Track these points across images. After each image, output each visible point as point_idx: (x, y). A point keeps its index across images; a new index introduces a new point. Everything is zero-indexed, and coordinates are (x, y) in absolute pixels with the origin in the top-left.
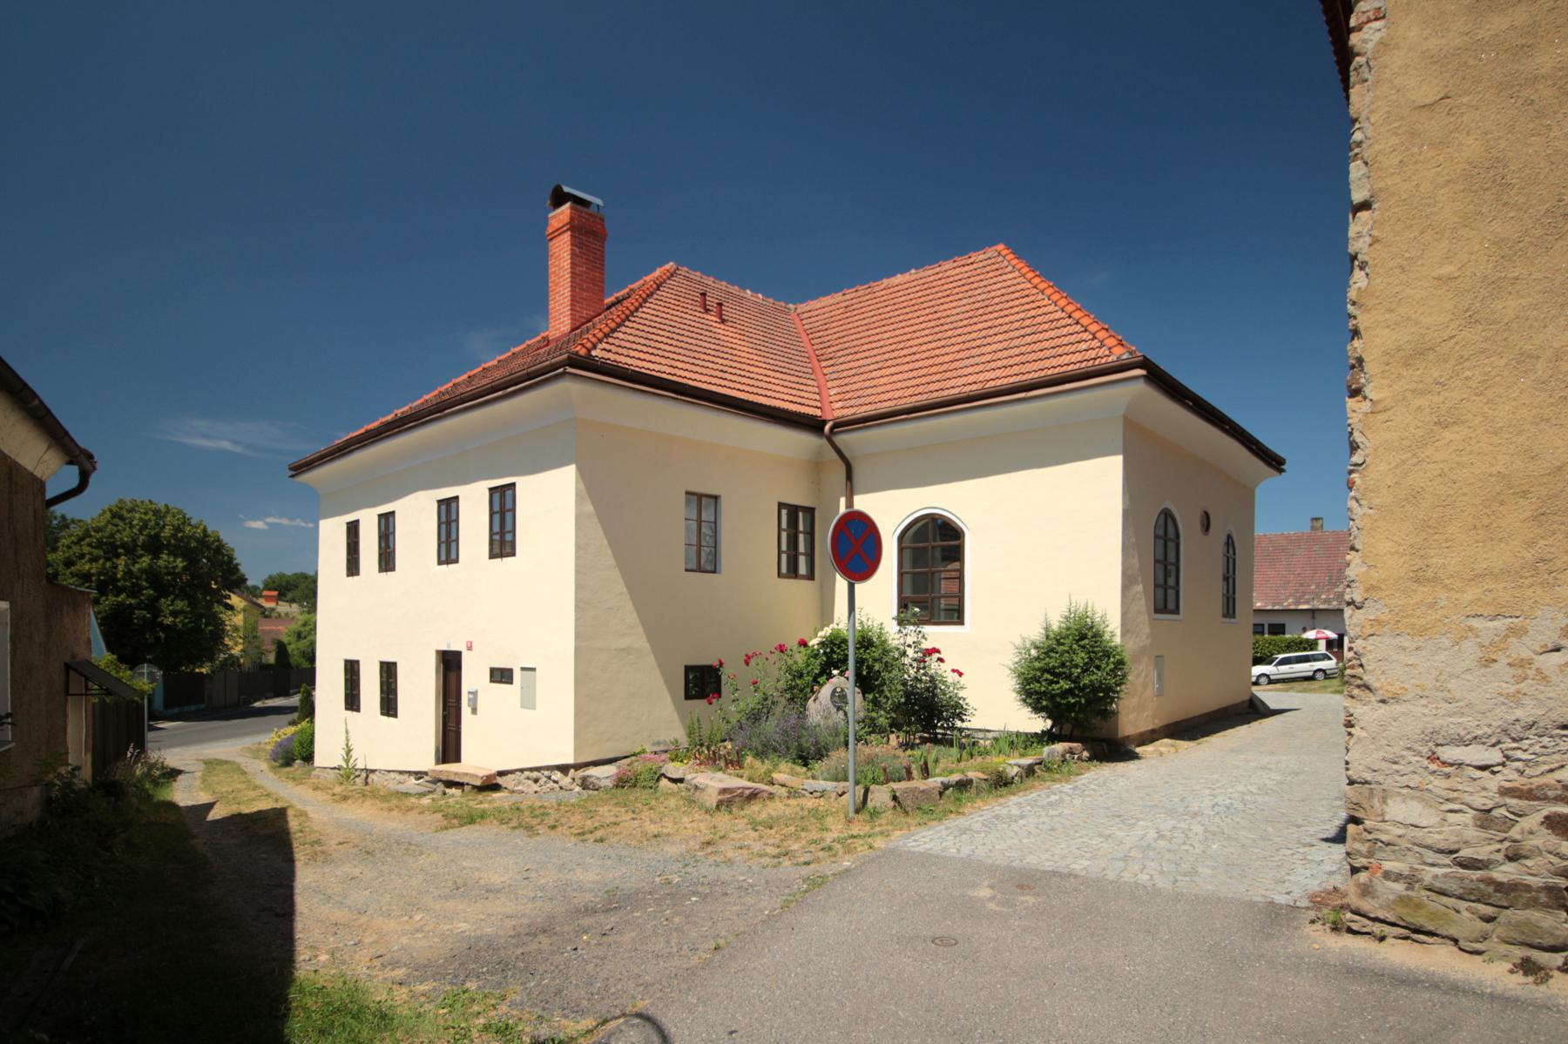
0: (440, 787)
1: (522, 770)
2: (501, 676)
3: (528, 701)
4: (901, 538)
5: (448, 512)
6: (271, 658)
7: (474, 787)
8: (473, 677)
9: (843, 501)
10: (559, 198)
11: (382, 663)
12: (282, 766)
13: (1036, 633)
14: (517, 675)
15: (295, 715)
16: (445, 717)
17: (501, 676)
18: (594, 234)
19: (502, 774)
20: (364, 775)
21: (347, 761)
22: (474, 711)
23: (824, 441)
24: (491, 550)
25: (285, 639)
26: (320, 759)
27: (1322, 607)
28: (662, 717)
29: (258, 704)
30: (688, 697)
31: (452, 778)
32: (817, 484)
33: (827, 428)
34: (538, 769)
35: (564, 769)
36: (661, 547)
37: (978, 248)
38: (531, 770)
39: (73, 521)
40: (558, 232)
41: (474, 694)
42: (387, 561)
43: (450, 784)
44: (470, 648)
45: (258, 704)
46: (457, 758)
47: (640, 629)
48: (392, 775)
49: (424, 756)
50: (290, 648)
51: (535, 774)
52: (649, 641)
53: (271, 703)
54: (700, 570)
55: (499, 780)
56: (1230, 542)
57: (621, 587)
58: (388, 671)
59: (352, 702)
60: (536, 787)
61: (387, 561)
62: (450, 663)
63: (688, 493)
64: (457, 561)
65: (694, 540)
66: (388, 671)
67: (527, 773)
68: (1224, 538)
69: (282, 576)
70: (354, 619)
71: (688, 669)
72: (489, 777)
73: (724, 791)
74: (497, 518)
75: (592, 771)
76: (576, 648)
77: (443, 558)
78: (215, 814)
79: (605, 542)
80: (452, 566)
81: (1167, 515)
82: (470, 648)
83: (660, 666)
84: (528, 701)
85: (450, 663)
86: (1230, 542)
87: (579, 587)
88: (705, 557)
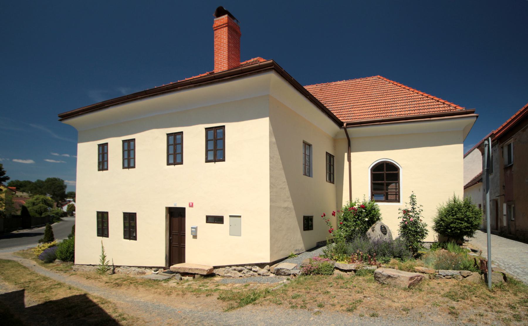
0: (179, 276)
1: (230, 266)
3: (235, 231)
5: (103, 150)
6: (19, 213)
7: (202, 275)
8: (193, 220)
9: (346, 154)
10: (220, 12)
11: (98, 213)
12: (46, 262)
14: (226, 220)
15: (42, 237)
16: (170, 240)
18: (237, 32)
19: (215, 268)
20: (112, 268)
21: (103, 263)
22: (195, 237)
23: (343, 130)
24: (99, 167)
25: (26, 205)
26: (78, 260)
28: (297, 238)
29: (15, 232)
30: (304, 230)
31: (187, 271)
32: (335, 147)
34: (243, 265)
35: (262, 265)
36: (305, 165)
37: (370, 76)
38: (237, 266)
40: (220, 27)
43: (185, 274)
45: (15, 232)
46: (182, 259)
47: (290, 199)
48: (133, 269)
49: (159, 258)
50: (29, 209)
51: (240, 268)
52: (294, 204)
53: (21, 231)
55: (215, 271)
57: (284, 179)
60: (240, 274)
62: (176, 216)
64: (134, 167)
67: (234, 268)
69: (18, 181)
70: (95, 188)
72: (211, 270)
73: (411, 278)
74: (126, 153)
75: (280, 266)
76: (270, 206)
77: (126, 165)
78: (31, 300)
79: (279, 157)
80: (131, 170)
83: (297, 216)
85: (176, 216)
87: (271, 177)
88: (308, 172)
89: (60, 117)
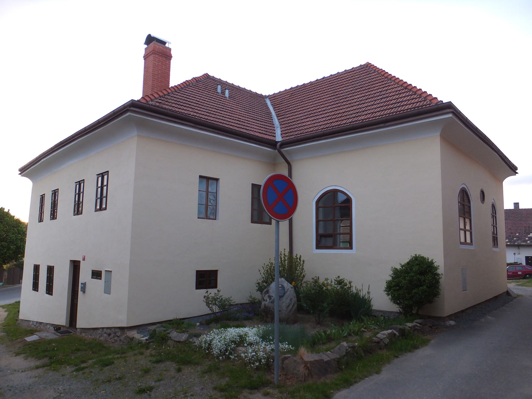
1: (103, 328)
2: (97, 275)
3: (107, 290)
4: (318, 202)
8: (85, 276)
13: (426, 256)
17: (97, 275)
22: (84, 292)
27: (522, 243)
33: (278, 144)
38: (107, 328)
39: (262, 288)
41: (84, 284)
42: (53, 216)
44: (84, 259)
49: (62, 320)
51: (109, 331)
54: (207, 218)
56: (493, 206)
58: (50, 270)
59: (36, 287)
61: (53, 216)
62: (75, 266)
63: (201, 177)
65: (204, 202)
66: (50, 270)
68: (491, 205)
71: (198, 272)
81: (464, 195)
82: (84, 259)
84: (107, 290)
85: (75, 266)
86: (493, 206)
89: (19, 171)
